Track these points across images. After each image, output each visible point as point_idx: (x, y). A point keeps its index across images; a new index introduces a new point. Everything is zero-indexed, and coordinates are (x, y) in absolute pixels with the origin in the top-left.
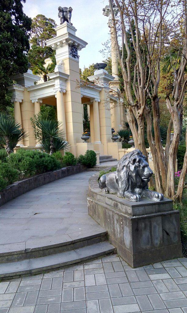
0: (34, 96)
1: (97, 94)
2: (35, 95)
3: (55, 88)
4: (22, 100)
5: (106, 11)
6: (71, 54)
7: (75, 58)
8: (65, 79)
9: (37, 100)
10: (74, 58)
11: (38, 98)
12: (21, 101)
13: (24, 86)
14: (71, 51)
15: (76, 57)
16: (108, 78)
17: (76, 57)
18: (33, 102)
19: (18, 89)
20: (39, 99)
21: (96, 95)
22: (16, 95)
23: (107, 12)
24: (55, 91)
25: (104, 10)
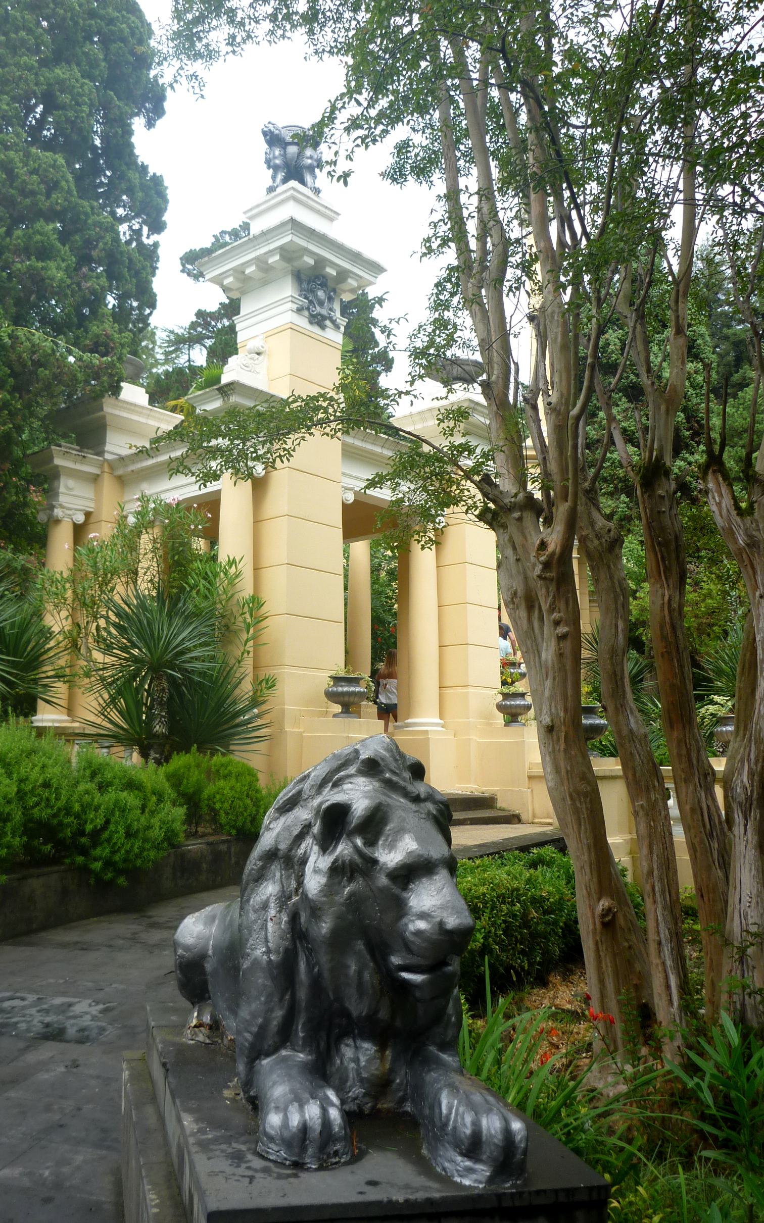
7: (323, 327)
10: (316, 329)
13: (100, 453)
14: (306, 298)
22: (62, 489)
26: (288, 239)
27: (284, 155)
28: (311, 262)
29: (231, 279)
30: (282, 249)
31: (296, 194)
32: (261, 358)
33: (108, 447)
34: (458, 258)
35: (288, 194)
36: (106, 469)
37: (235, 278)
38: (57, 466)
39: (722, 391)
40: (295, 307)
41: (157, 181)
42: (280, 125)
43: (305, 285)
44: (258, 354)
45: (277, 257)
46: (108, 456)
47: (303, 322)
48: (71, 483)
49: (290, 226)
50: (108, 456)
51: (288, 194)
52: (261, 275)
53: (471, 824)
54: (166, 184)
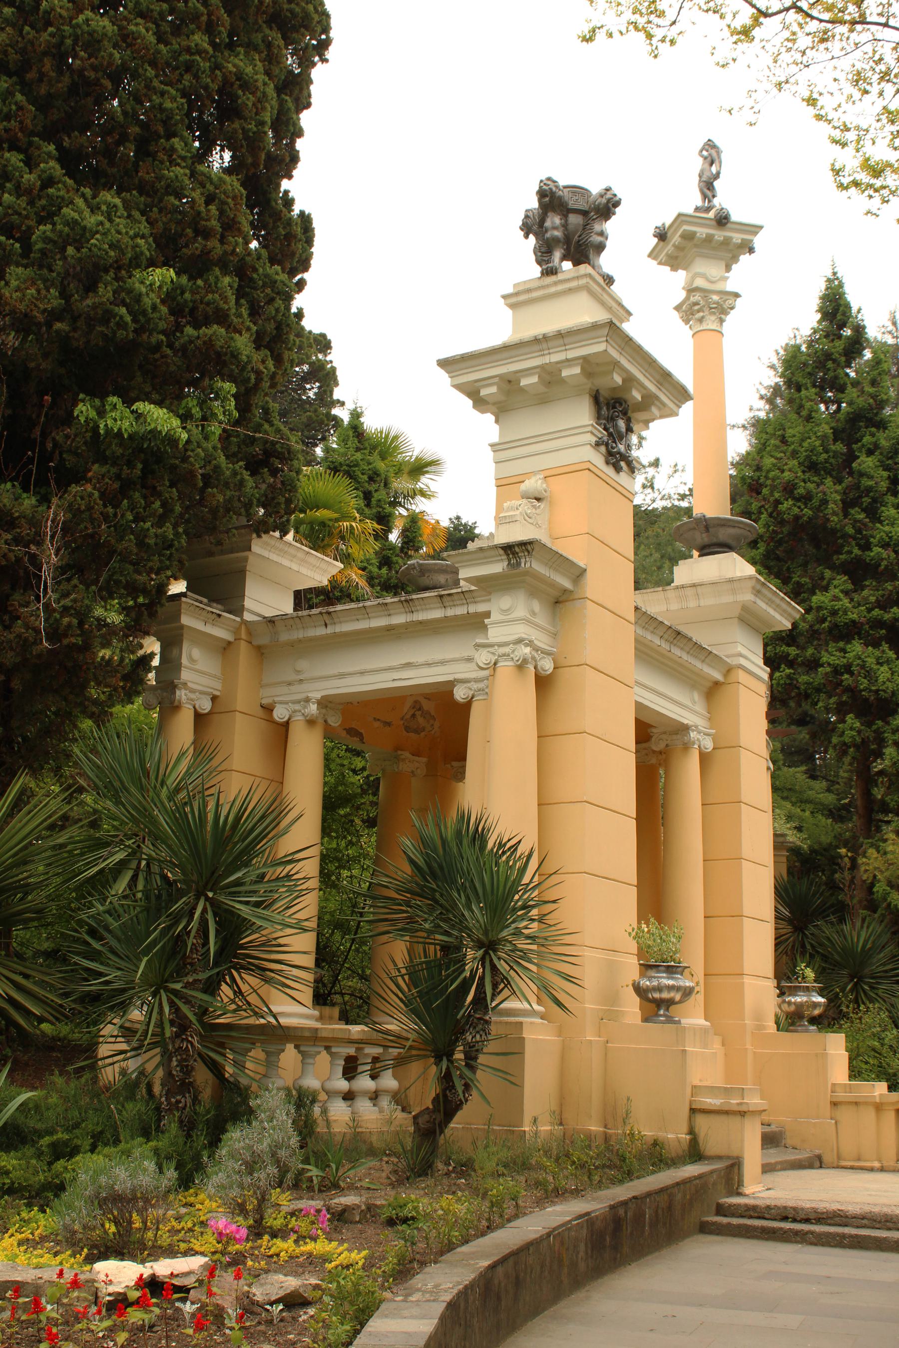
0: (293, 677)
1: (694, 703)
2: (298, 672)
3: (492, 640)
4: (214, 699)
5: (676, 239)
6: (603, 449)
7: (618, 469)
8: (553, 585)
9: (313, 708)
10: (610, 471)
11: (318, 695)
12: (206, 706)
13: (238, 610)
14: (605, 429)
15: (623, 464)
16: (772, 612)
17: (623, 464)
18: (280, 714)
19: (199, 625)
20: (325, 703)
21: (690, 704)
22: (184, 661)
23: (678, 248)
24: (484, 657)
25: (662, 235)
26: (601, 347)
27: (565, 226)
28: (618, 379)
29: (493, 389)
30: (585, 360)
31: (591, 283)
32: (542, 505)
33: (248, 603)
34: (286, 192)
35: (582, 282)
36: (243, 635)
37: (499, 388)
38: (182, 627)
39: (866, 500)
40: (593, 440)
41: (305, 220)
42: (562, 183)
43: (604, 411)
44: (538, 499)
45: (577, 370)
46: (247, 616)
47: (598, 459)
48: (196, 653)
49: (605, 331)
50: (247, 616)
51: (582, 282)
52: (542, 389)
53: (734, 1235)
54: (314, 225)
